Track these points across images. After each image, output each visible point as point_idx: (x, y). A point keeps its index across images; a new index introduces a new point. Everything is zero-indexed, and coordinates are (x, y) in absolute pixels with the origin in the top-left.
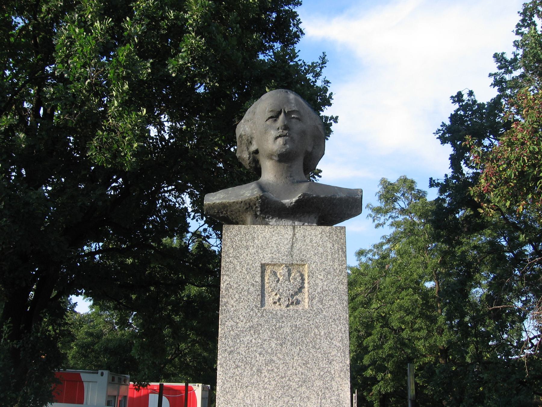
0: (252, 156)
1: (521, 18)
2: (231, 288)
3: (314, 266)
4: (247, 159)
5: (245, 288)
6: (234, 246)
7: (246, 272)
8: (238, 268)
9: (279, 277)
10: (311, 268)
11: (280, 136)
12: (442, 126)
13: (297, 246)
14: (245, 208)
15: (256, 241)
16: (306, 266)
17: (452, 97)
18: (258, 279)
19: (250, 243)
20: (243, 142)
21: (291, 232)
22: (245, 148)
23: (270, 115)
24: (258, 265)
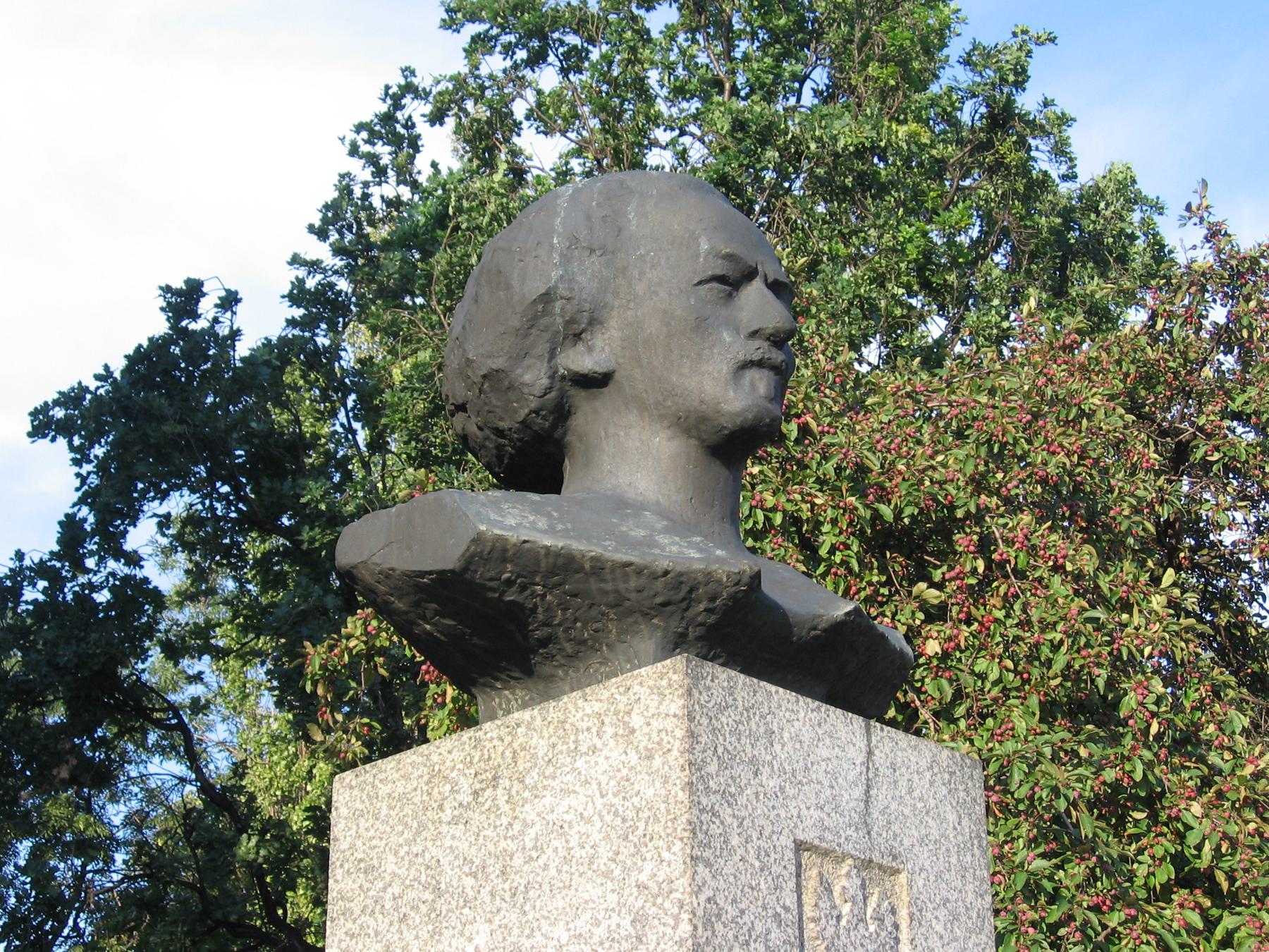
0: (558, 385)
1: (383, 108)
2: (719, 916)
3: (921, 883)
4: (538, 391)
5: (759, 927)
6: (720, 750)
7: (757, 864)
8: (735, 841)
9: (838, 902)
10: (915, 889)
11: (759, 364)
12: (98, 377)
13: (881, 795)
14: (658, 600)
15: (777, 747)
16: (903, 878)
17: (167, 289)
18: (790, 900)
19: (760, 752)
20: (545, 321)
21: (862, 743)
22: (542, 348)
23: (719, 268)
24: (786, 841)
